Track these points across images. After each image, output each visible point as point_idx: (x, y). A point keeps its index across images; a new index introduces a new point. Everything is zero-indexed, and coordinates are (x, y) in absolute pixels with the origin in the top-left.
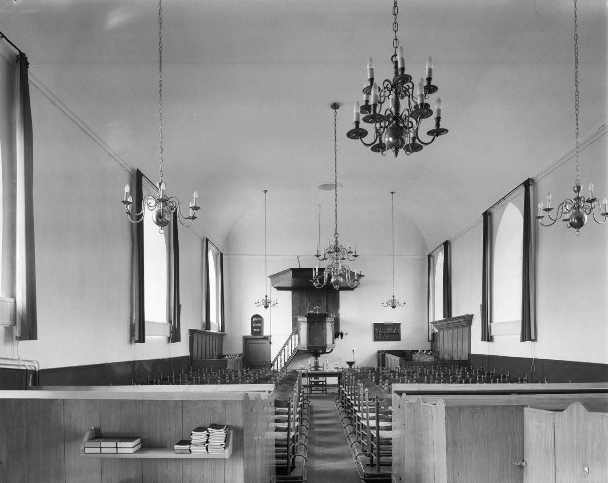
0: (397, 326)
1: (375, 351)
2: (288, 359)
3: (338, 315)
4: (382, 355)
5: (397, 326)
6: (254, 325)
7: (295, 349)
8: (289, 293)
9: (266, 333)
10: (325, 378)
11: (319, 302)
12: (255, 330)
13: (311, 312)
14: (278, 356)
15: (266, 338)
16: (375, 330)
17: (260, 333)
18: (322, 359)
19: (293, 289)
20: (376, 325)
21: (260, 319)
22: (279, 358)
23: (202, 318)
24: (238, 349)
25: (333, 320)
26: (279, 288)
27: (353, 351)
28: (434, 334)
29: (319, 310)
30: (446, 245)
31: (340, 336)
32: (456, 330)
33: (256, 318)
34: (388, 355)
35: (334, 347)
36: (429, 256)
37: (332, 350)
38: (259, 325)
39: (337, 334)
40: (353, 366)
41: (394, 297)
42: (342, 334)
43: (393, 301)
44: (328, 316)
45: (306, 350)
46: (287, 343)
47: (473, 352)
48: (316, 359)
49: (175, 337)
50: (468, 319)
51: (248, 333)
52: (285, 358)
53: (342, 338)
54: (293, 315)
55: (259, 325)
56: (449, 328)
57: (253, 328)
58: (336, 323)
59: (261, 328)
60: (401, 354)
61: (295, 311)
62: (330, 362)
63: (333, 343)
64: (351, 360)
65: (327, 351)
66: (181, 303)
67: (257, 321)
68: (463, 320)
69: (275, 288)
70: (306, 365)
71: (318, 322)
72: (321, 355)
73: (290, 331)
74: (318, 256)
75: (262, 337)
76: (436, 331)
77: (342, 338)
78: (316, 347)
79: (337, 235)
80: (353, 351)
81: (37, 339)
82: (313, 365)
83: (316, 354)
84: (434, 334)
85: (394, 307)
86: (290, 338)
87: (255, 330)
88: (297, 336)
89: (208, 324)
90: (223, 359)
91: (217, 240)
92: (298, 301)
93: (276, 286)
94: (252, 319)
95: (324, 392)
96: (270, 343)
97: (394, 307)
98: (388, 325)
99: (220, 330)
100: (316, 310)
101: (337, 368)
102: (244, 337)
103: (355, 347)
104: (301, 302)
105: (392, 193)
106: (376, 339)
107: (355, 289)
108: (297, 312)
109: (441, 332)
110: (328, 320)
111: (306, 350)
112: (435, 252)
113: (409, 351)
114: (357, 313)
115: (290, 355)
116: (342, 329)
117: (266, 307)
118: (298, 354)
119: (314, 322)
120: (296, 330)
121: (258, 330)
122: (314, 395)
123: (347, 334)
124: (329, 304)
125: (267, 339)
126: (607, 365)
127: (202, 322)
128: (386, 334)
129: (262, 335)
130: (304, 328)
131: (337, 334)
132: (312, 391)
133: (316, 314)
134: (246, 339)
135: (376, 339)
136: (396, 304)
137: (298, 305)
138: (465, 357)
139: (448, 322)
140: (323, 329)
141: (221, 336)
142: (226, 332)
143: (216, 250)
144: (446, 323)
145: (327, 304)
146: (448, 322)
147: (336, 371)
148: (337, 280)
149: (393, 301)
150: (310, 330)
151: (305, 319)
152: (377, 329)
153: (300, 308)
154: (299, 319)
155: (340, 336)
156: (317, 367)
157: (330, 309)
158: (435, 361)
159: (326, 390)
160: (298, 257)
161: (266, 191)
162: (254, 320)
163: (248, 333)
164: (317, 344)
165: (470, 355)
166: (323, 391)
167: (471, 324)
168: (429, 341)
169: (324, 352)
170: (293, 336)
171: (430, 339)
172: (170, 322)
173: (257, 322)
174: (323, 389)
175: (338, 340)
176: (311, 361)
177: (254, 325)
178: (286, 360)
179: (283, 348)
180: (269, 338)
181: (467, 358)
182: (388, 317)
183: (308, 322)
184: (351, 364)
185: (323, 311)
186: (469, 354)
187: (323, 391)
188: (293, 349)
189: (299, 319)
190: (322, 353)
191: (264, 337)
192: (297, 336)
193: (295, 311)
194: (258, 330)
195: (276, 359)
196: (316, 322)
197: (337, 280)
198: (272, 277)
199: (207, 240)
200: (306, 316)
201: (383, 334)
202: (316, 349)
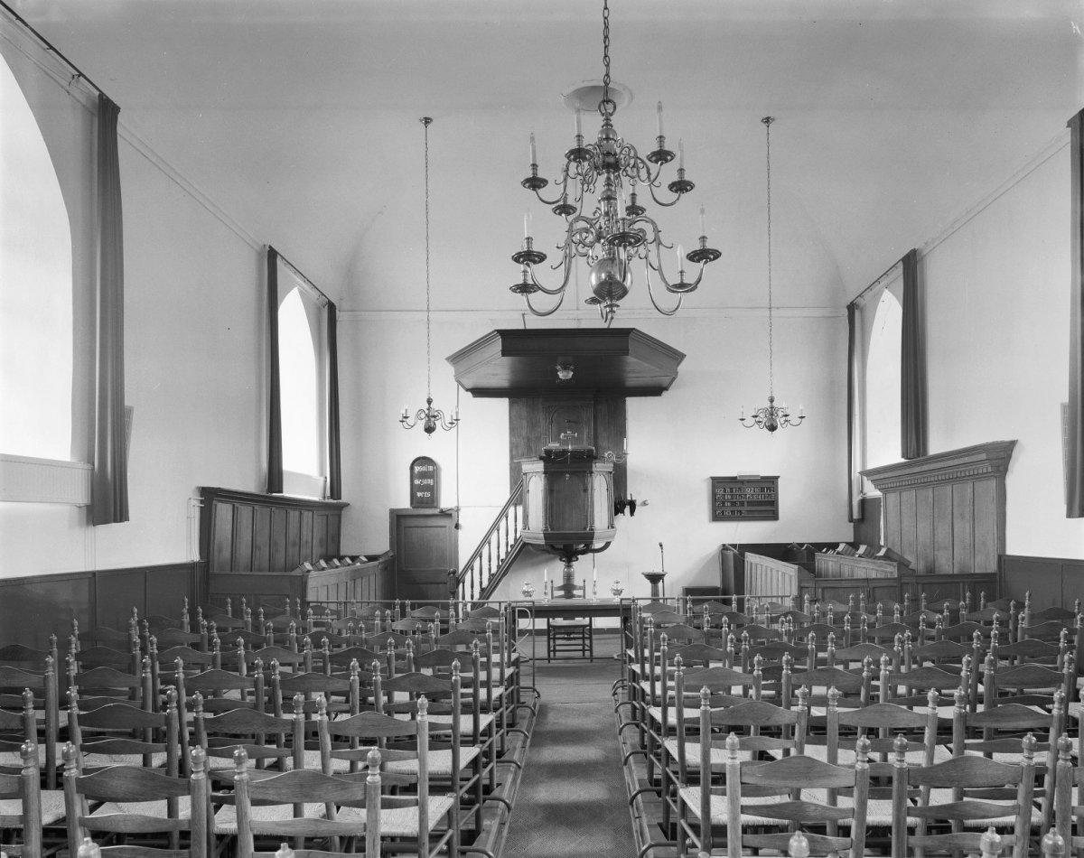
0: (770, 483)
1: (714, 548)
2: (499, 567)
3: (622, 455)
4: (734, 559)
5: (770, 483)
6: (417, 482)
7: (516, 540)
8: (502, 404)
9: (446, 502)
10: (587, 619)
11: (574, 424)
12: (419, 494)
13: (554, 446)
14: (473, 559)
15: (446, 514)
16: (714, 495)
17: (432, 501)
18: (582, 565)
19: (512, 392)
20: (717, 482)
21: (431, 468)
22: (476, 564)
23: (259, 461)
24: (380, 542)
25: (610, 467)
26: (479, 392)
27: (661, 546)
28: (864, 503)
29: (575, 441)
30: (911, 265)
31: (627, 510)
32: (949, 488)
33: (422, 465)
34: (750, 558)
35: (613, 537)
36: (852, 308)
37: (608, 544)
38: (430, 482)
39: (622, 505)
40: (660, 584)
41: (772, 400)
42: (632, 505)
43: (772, 412)
44: (596, 458)
45: (542, 542)
46: (495, 526)
47: (1013, 549)
48: (569, 566)
49: (107, 503)
50: (998, 458)
51: (404, 503)
52: (488, 563)
53: (632, 513)
54: (512, 458)
55: (430, 482)
56: (919, 484)
57: (413, 489)
58: (619, 477)
59: (433, 490)
60: (782, 552)
61: (517, 447)
62: (607, 576)
63: (612, 526)
64: (658, 570)
65: (597, 545)
66: (128, 401)
67: (425, 471)
68: (983, 456)
69: (467, 390)
70: (540, 584)
71: (572, 474)
72: (579, 556)
73: (504, 494)
74: (535, 183)
75: (437, 511)
76: (877, 493)
77: (632, 513)
78: (565, 537)
79: (610, 107)
80: (661, 546)
81: (127, 519)
82: (560, 582)
83: (569, 555)
84: (864, 503)
85: (772, 428)
86: (504, 513)
87: (419, 494)
88: (520, 509)
89: (275, 476)
90: (297, 572)
91: (310, 252)
92: (525, 423)
93: (470, 384)
94: (412, 468)
95: (587, 653)
96: (457, 526)
97: (772, 428)
98: (749, 481)
99: (328, 493)
100: (564, 441)
101: (618, 592)
102: (392, 512)
103: (660, 541)
104: (533, 425)
105: (767, 120)
106: (718, 515)
107: (665, 393)
108: (519, 451)
109: (892, 498)
110: (598, 467)
111: (542, 542)
112: (868, 296)
113: (801, 545)
114: (672, 452)
115: (503, 556)
116: (633, 491)
117: (429, 430)
118: (524, 554)
119: (563, 473)
120: (518, 496)
121: (428, 495)
122: (561, 663)
123: (644, 504)
124: (600, 430)
125: (450, 515)
126: (1070, 566)
127: (260, 469)
128: (742, 504)
129: (436, 507)
130: (536, 488)
131: (622, 505)
132: (555, 651)
133: (565, 452)
134: (398, 518)
135: (718, 515)
136: (779, 421)
137: (524, 433)
138: (986, 563)
139: (917, 469)
140: (586, 490)
141: (332, 510)
142: (345, 497)
143: (314, 294)
144: (908, 471)
145: (595, 430)
146: (917, 469)
147: (616, 600)
148: (610, 276)
149: (772, 412)
150: (550, 491)
151: (540, 466)
152: (720, 492)
153: (529, 440)
154: (526, 467)
155: (627, 510)
156: (568, 588)
157: (603, 443)
158: (900, 577)
159: (591, 650)
160: (523, 315)
161: (427, 121)
162: (417, 469)
163: (404, 503)
164: (570, 527)
165: (1003, 559)
166: (584, 650)
167: (1006, 470)
168: (851, 520)
169: (588, 549)
170: (512, 510)
171: (856, 515)
172: (90, 461)
173: (423, 475)
174: (584, 645)
175: (623, 519)
176: (553, 572)
177: (417, 482)
178: (494, 570)
179: (486, 540)
180: (454, 514)
181: (992, 567)
182: (750, 456)
183: (545, 473)
184: (655, 578)
185: (586, 445)
186: (1000, 557)
187: (584, 650)
188: (511, 542)
189: (526, 467)
190: (583, 552)
191: (442, 511)
192: (520, 509)
193: (517, 447)
194: (428, 495)
195: (469, 566)
196: (567, 472)
197: (610, 276)
198: (456, 359)
199: (272, 255)
200: (541, 458)
201: (733, 504)
202: (567, 541)
